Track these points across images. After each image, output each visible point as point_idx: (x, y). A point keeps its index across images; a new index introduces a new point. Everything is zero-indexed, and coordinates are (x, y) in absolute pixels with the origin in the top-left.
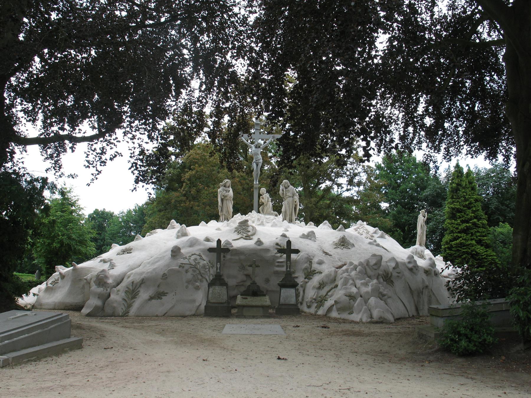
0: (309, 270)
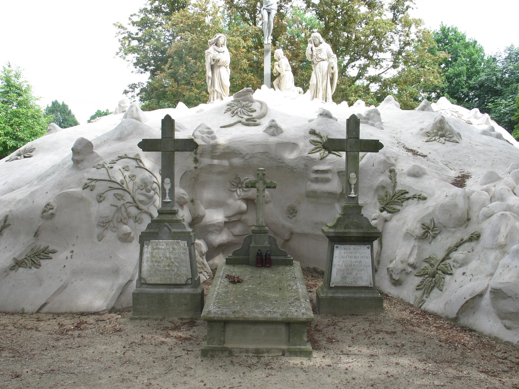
0: (391, 192)
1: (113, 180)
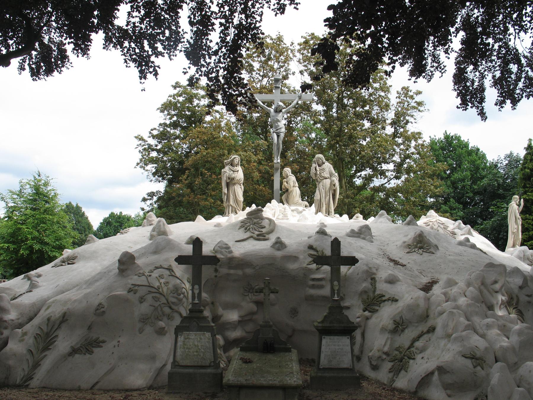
0: (371, 295)
1: (152, 285)
